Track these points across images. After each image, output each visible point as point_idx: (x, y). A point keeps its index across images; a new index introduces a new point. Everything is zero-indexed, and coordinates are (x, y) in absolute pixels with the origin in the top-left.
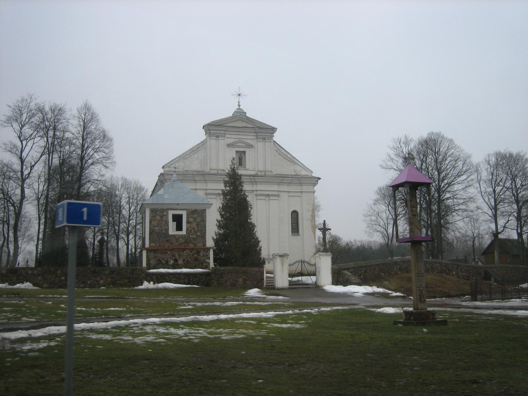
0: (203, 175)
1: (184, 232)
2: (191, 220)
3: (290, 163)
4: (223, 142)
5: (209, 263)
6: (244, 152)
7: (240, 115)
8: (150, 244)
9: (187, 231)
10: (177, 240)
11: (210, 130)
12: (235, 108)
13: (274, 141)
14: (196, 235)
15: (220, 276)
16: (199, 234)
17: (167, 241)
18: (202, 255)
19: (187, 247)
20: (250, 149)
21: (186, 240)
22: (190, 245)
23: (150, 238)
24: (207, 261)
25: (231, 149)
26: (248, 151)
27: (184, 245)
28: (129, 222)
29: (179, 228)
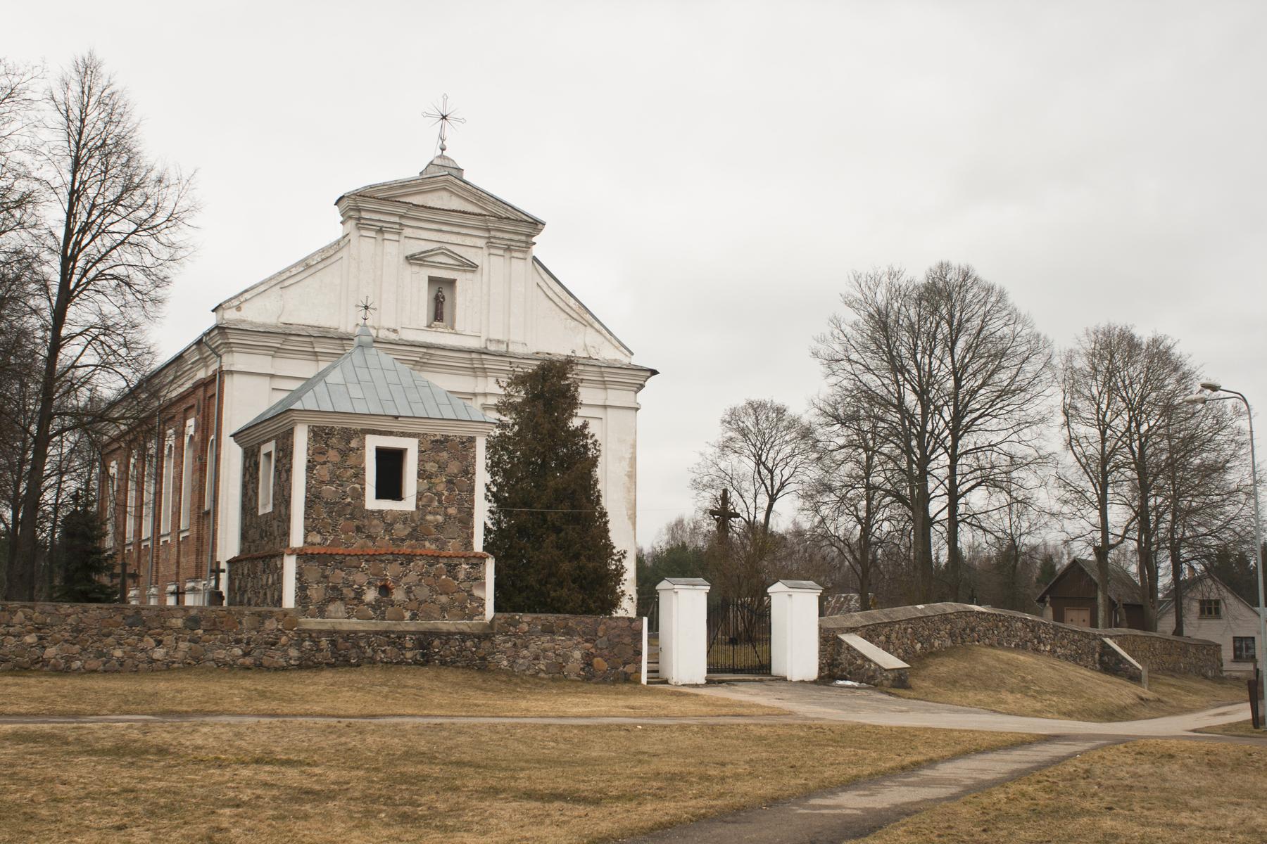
0: (341, 339)
1: (408, 504)
2: (431, 467)
3: (574, 323)
4: (394, 250)
5: (481, 602)
6: (451, 283)
7: (444, 175)
8: (306, 537)
9: (418, 499)
10: (389, 527)
11: (359, 210)
12: (432, 153)
13: (535, 259)
14: (446, 515)
15: (519, 642)
16: (452, 511)
17: (359, 529)
18: (462, 576)
19: (419, 551)
20: (469, 275)
21: (414, 529)
22: (427, 544)
23: (307, 516)
24: (477, 593)
25: (416, 269)
26: (462, 279)
27: (407, 543)
28: (956, 439)
29: (390, 486)
